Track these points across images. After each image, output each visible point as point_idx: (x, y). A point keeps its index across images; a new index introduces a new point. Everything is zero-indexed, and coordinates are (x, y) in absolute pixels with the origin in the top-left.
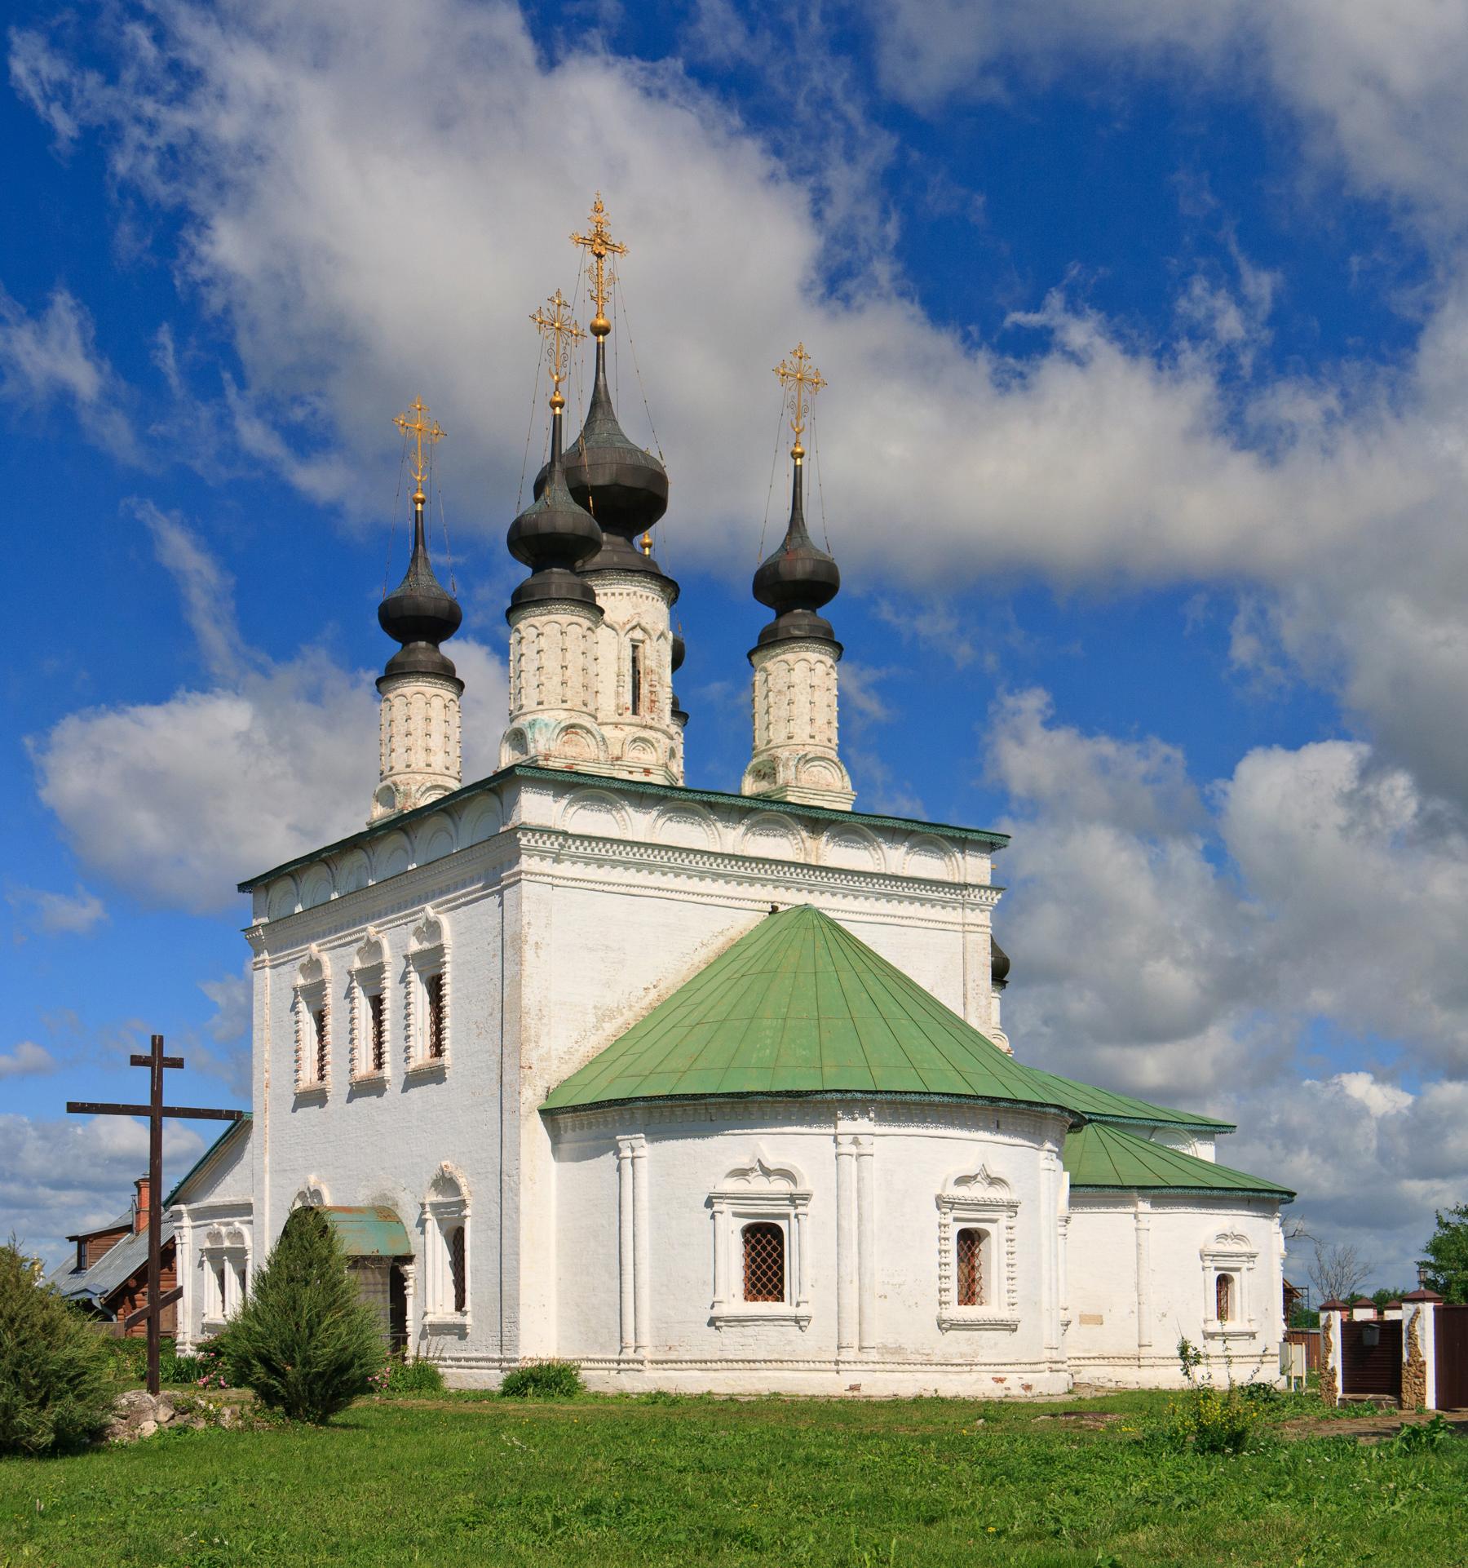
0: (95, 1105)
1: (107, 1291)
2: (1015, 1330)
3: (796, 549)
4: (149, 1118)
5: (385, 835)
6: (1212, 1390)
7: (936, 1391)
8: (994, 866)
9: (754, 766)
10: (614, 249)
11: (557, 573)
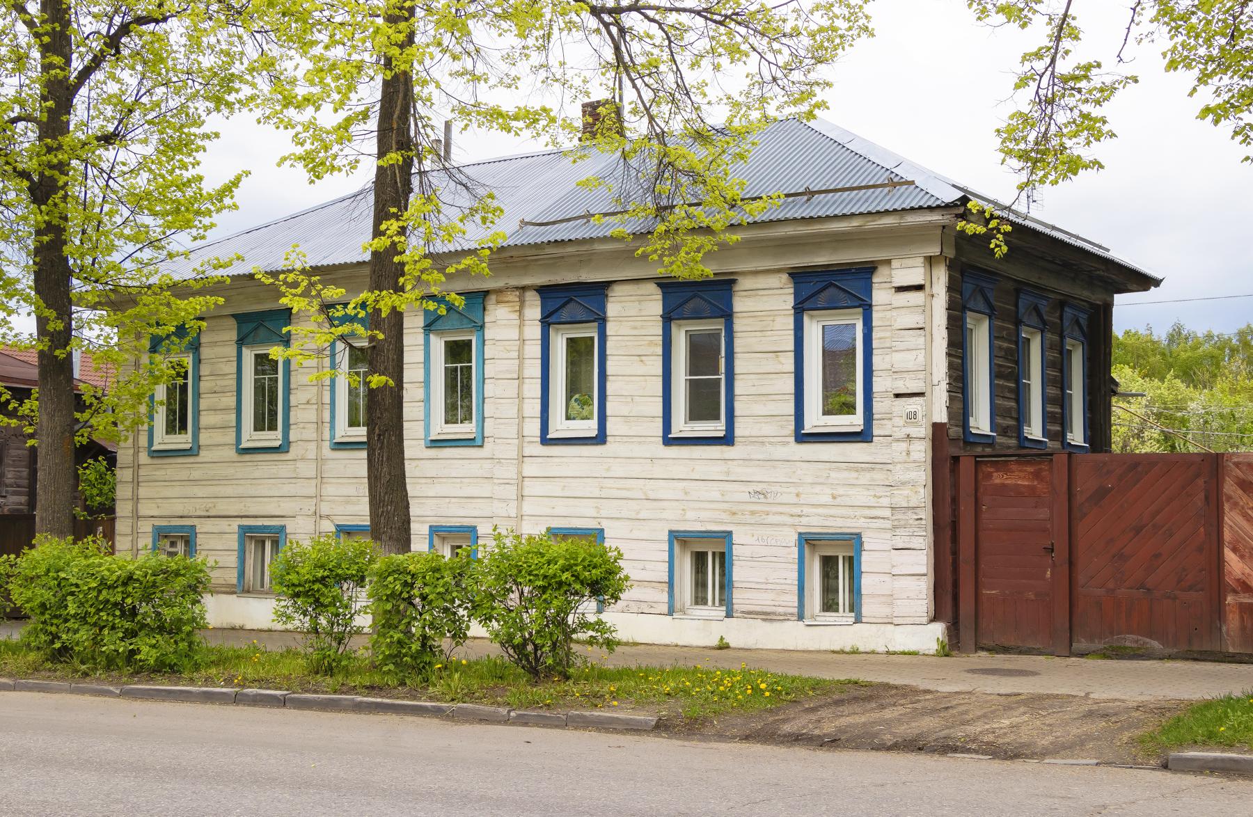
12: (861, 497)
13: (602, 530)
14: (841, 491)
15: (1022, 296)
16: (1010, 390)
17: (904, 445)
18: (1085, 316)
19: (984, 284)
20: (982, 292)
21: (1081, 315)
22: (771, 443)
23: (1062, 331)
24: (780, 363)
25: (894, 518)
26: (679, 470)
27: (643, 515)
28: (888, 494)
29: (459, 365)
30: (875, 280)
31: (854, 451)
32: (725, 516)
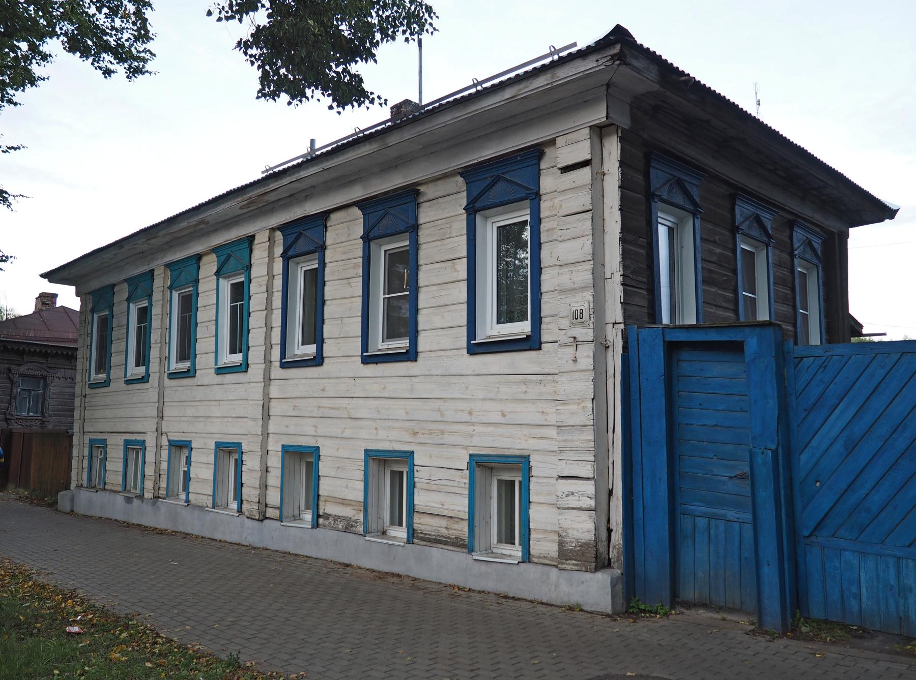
12: (529, 414)
13: (318, 448)
14: (509, 407)
15: (738, 202)
16: (727, 300)
17: (570, 351)
18: (819, 241)
19: (683, 177)
20: (680, 184)
21: (813, 238)
22: (447, 356)
23: (792, 250)
24: (456, 270)
25: (560, 438)
26: (374, 388)
27: (347, 434)
28: (554, 410)
29: (238, 303)
30: (543, 165)
31: (523, 360)
32: (408, 438)
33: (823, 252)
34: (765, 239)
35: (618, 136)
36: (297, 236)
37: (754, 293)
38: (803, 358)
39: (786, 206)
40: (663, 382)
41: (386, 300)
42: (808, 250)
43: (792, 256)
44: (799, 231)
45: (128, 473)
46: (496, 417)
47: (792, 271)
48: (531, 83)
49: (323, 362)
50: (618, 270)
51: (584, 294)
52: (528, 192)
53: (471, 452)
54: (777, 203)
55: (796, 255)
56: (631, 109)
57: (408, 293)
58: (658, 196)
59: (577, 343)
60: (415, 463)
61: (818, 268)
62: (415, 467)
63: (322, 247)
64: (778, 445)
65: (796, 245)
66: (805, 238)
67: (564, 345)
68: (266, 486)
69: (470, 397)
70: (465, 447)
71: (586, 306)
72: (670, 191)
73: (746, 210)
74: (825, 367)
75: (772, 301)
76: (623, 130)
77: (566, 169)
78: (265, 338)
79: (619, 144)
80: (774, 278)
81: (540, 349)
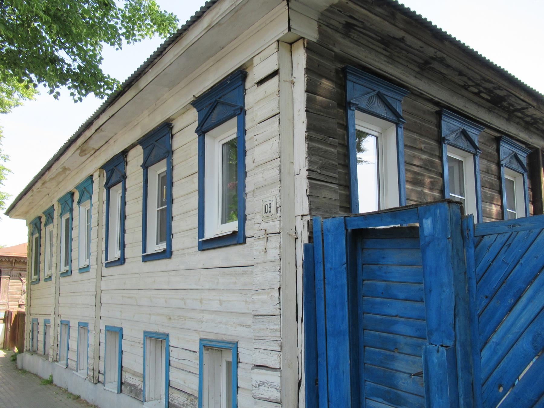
0: (401, 192)
1: (361, 159)
2: (193, 96)
3: (429, 236)
4: (93, 93)
5: (535, 133)
6: (37, 375)
7: (306, 132)
8: (310, 236)
9: (430, 191)
10: (121, 48)
11: (467, 213)
13: (121, 329)
15: (444, 118)
17: (262, 242)
20: (380, 96)
33: (529, 164)
34: (473, 150)
35: (304, 47)
36: (111, 173)
37: (462, 194)
38: (483, 236)
39: (492, 124)
40: (345, 271)
41: (159, 212)
42: (514, 161)
43: (499, 165)
44: (506, 146)
45: (46, 343)
46: (215, 306)
47: (499, 178)
48: (220, 9)
49: (125, 262)
50: (305, 166)
51: (273, 190)
52: (234, 108)
53: (202, 337)
54: (483, 122)
55: (502, 165)
56: (319, 26)
57: (166, 206)
58: (354, 104)
59: (268, 236)
60: (170, 344)
61: (523, 175)
62: (170, 347)
63: (123, 177)
64: (455, 341)
65: (502, 157)
66: (511, 152)
67: (259, 238)
68: (99, 357)
69: (200, 288)
70: (198, 331)
71: (274, 200)
72: (370, 100)
73: (452, 126)
74: (510, 245)
75: (480, 200)
76: (309, 42)
77: (261, 82)
78: (97, 246)
79: (306, 54)
80: (481, 181)
81: (244, 243)
